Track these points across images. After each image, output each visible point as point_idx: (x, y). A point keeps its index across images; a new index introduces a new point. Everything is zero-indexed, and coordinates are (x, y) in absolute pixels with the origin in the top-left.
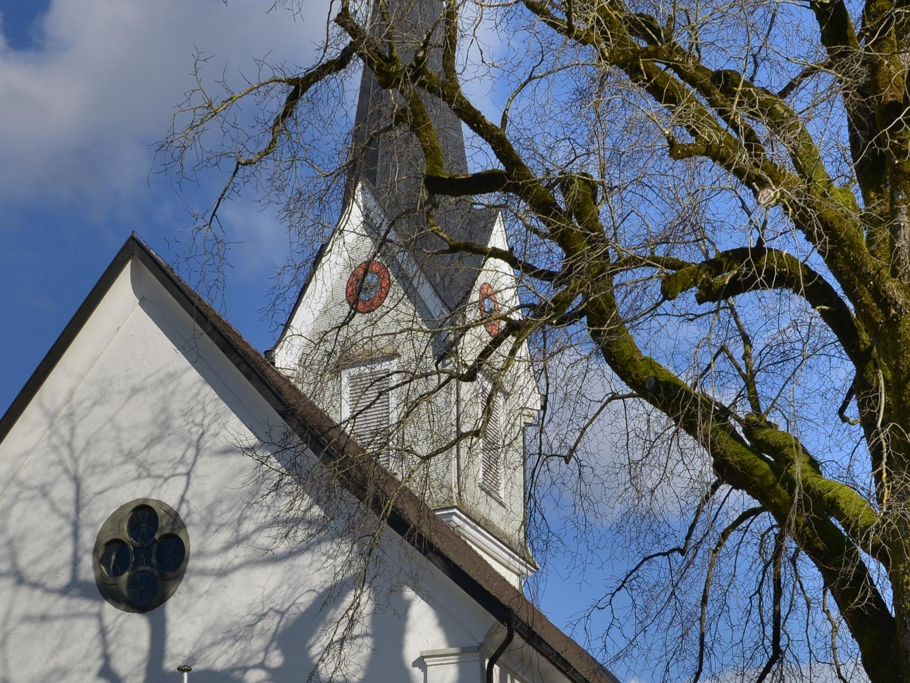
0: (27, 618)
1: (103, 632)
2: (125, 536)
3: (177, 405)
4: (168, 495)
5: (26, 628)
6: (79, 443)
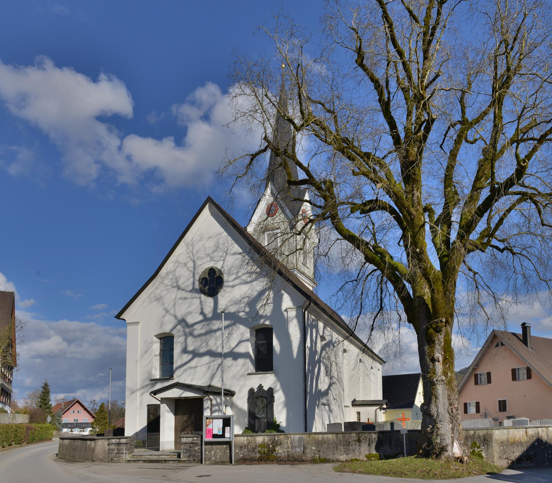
0: (181, 299)
1: (201, 302)
3: (221, 242)
4: (219, 266)
5: (180, 301)
6: (195, 252)
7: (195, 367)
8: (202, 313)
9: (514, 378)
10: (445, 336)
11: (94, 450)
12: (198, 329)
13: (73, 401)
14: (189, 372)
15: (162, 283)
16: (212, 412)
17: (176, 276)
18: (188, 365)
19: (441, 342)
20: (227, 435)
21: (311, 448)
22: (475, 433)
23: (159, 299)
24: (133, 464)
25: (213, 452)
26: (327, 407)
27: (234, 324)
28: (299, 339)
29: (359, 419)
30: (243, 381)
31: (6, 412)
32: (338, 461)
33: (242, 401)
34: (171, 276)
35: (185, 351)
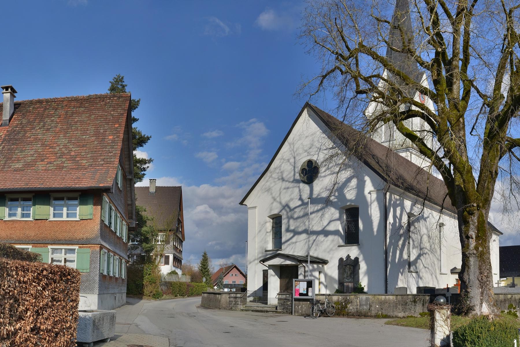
0: (285, 189)
1: (300, 190)
2: (306, 168)
3: (316, 139)
4: (314, 158)
5: (285, 191)
6: (295, 150)
7: (296, 242)
8: (301, 199)
10: (479, 218)
11: (220, 301)
12: (298, 213)
13: (232, 266)
14: (291, 246)
15: (271, 176)
16: (305, 276)
17: (282, 170)
18: (291, 241)
19: (475, 223)
20: (310, 294)
21: (376, 306)
22: (512, 296)
23: (269, 190)
24: (245, 312)
25: (300, 307)
26: (414, 274)
27: (327, 206)
28: (379, 218)
30: (334, 252)
31: (177, 273)
32: (396, 317)
33: (332, 270)
34: (277, 171)
35: (288, 230)
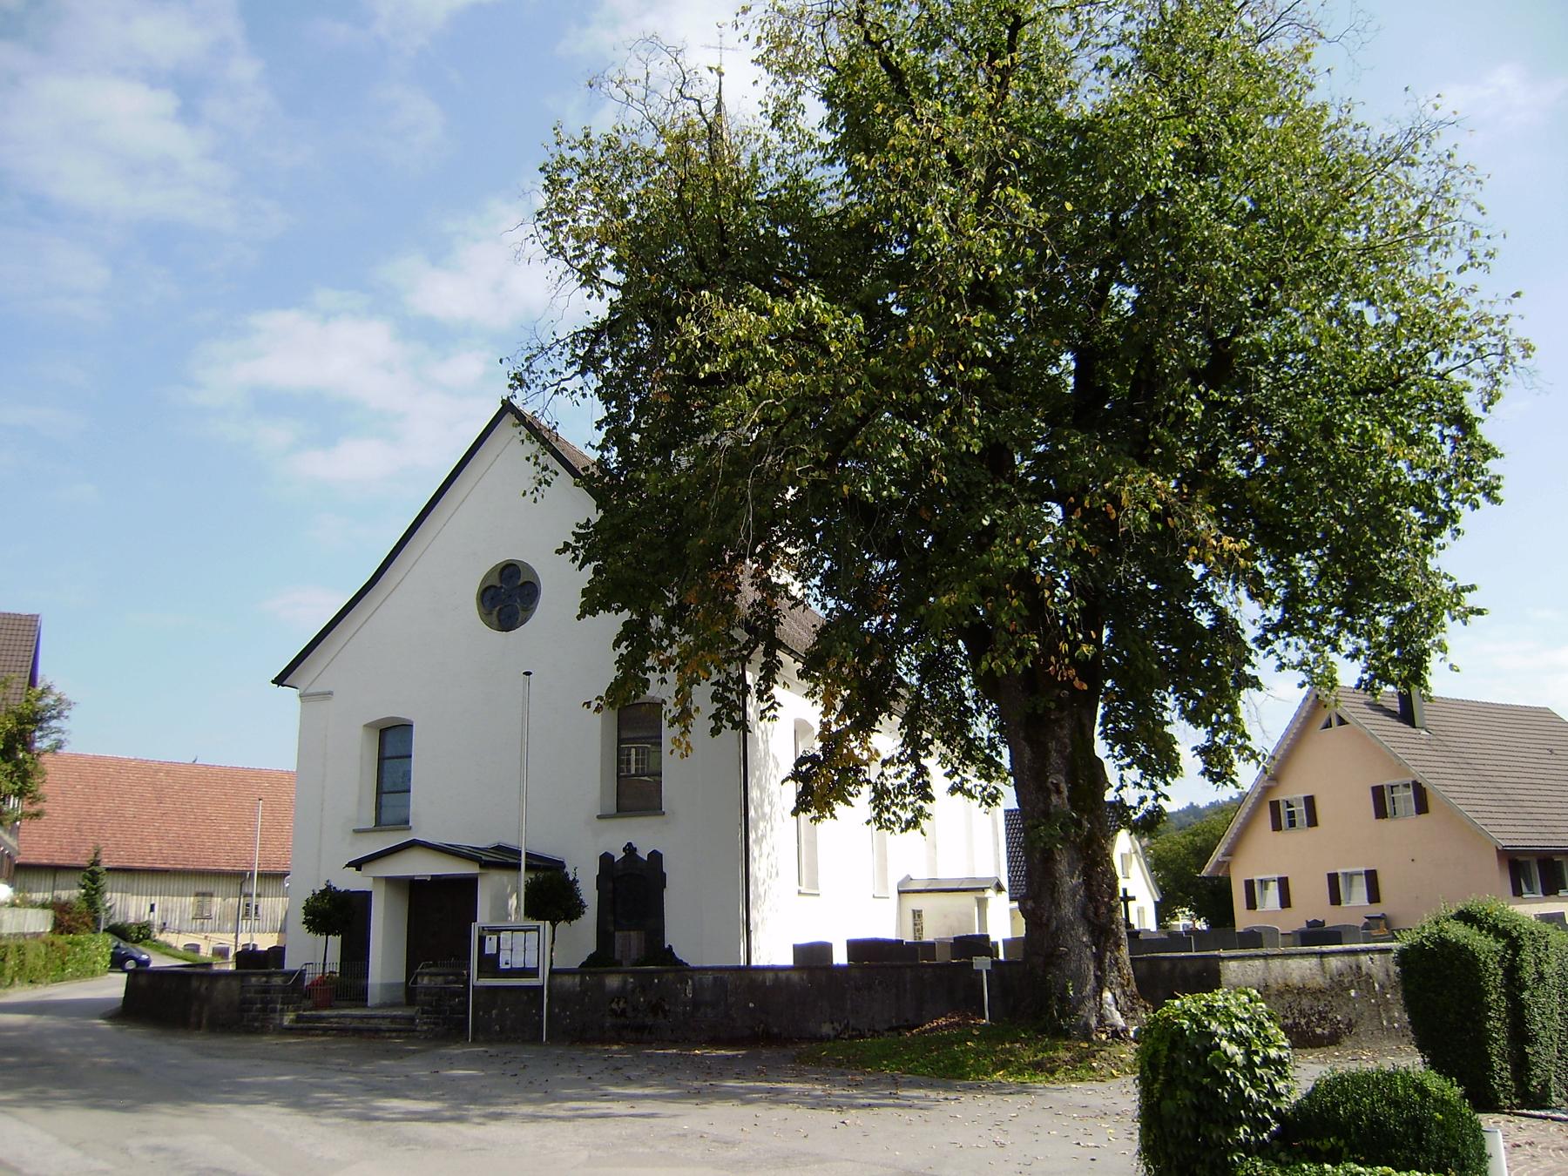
9: (1381, 812)
29: (918, 928)
